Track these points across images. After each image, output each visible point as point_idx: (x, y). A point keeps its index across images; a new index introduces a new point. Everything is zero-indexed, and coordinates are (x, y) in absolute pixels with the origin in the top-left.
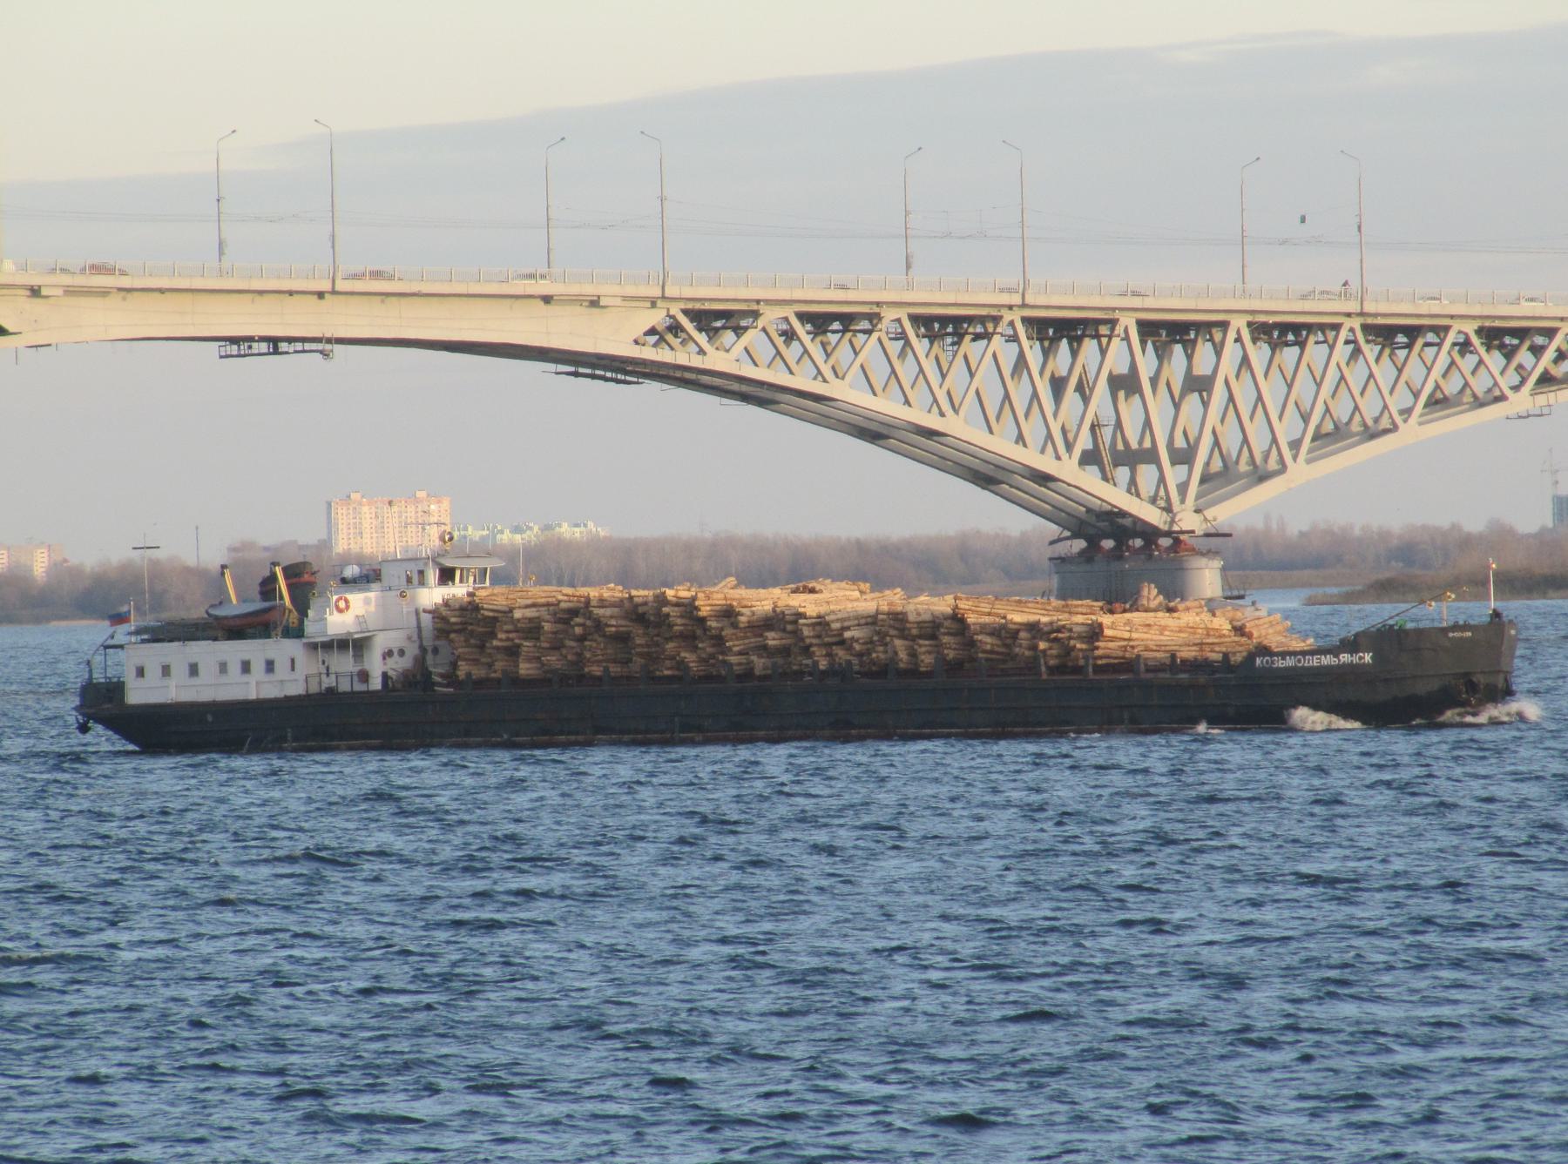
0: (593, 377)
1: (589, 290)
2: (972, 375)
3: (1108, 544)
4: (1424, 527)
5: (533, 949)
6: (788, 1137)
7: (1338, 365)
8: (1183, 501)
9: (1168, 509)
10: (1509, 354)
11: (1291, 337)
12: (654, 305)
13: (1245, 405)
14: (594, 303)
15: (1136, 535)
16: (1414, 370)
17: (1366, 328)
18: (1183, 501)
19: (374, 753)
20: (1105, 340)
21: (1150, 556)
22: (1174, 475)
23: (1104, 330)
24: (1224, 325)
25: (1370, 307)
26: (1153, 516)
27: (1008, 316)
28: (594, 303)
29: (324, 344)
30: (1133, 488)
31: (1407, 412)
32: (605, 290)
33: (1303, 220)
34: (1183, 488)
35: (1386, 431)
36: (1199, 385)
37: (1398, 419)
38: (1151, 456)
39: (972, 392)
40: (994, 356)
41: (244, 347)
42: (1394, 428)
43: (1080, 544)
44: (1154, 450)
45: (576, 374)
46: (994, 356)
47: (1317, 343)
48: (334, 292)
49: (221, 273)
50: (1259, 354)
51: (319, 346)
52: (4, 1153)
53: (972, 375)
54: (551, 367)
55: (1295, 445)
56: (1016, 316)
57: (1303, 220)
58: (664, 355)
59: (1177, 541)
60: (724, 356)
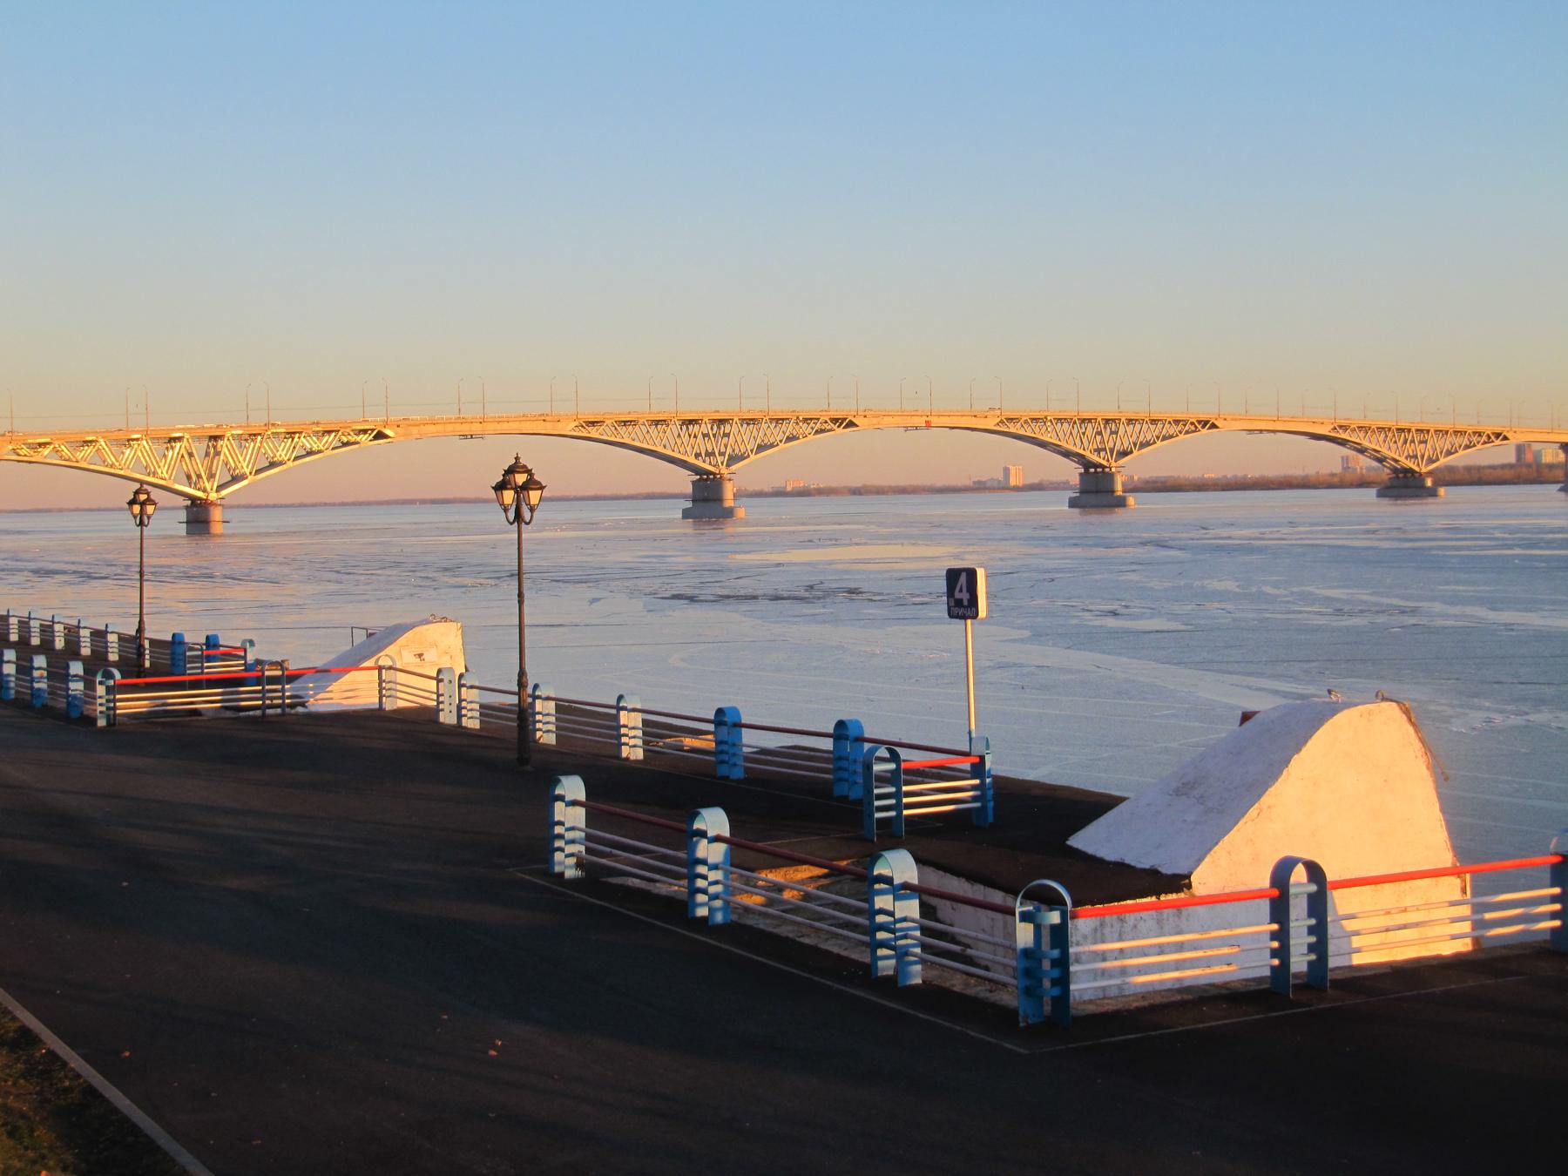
1: (1321, 421)
4: (1285, 477)
6: (14, 563)
9: (1108, 460)
10: (808, 424)
13: (739, 441)
14: (1322, 423)
15: (1409, 472)
16: (784, 428)
19: (1387, 499)
21: (1415, 477)
22: (720, 459)
23: (1117, 421)
24: (702, 420)
26: (1417, 469)
28: (1322, 423)
32: (1325, 421)
34: (722, 463)
36: (728, 435)
42: (778, 445)
43: (1394, 475)
44: (714, 453)
52: (9, 543)
56: (1076, 418)
60: (594, 432)
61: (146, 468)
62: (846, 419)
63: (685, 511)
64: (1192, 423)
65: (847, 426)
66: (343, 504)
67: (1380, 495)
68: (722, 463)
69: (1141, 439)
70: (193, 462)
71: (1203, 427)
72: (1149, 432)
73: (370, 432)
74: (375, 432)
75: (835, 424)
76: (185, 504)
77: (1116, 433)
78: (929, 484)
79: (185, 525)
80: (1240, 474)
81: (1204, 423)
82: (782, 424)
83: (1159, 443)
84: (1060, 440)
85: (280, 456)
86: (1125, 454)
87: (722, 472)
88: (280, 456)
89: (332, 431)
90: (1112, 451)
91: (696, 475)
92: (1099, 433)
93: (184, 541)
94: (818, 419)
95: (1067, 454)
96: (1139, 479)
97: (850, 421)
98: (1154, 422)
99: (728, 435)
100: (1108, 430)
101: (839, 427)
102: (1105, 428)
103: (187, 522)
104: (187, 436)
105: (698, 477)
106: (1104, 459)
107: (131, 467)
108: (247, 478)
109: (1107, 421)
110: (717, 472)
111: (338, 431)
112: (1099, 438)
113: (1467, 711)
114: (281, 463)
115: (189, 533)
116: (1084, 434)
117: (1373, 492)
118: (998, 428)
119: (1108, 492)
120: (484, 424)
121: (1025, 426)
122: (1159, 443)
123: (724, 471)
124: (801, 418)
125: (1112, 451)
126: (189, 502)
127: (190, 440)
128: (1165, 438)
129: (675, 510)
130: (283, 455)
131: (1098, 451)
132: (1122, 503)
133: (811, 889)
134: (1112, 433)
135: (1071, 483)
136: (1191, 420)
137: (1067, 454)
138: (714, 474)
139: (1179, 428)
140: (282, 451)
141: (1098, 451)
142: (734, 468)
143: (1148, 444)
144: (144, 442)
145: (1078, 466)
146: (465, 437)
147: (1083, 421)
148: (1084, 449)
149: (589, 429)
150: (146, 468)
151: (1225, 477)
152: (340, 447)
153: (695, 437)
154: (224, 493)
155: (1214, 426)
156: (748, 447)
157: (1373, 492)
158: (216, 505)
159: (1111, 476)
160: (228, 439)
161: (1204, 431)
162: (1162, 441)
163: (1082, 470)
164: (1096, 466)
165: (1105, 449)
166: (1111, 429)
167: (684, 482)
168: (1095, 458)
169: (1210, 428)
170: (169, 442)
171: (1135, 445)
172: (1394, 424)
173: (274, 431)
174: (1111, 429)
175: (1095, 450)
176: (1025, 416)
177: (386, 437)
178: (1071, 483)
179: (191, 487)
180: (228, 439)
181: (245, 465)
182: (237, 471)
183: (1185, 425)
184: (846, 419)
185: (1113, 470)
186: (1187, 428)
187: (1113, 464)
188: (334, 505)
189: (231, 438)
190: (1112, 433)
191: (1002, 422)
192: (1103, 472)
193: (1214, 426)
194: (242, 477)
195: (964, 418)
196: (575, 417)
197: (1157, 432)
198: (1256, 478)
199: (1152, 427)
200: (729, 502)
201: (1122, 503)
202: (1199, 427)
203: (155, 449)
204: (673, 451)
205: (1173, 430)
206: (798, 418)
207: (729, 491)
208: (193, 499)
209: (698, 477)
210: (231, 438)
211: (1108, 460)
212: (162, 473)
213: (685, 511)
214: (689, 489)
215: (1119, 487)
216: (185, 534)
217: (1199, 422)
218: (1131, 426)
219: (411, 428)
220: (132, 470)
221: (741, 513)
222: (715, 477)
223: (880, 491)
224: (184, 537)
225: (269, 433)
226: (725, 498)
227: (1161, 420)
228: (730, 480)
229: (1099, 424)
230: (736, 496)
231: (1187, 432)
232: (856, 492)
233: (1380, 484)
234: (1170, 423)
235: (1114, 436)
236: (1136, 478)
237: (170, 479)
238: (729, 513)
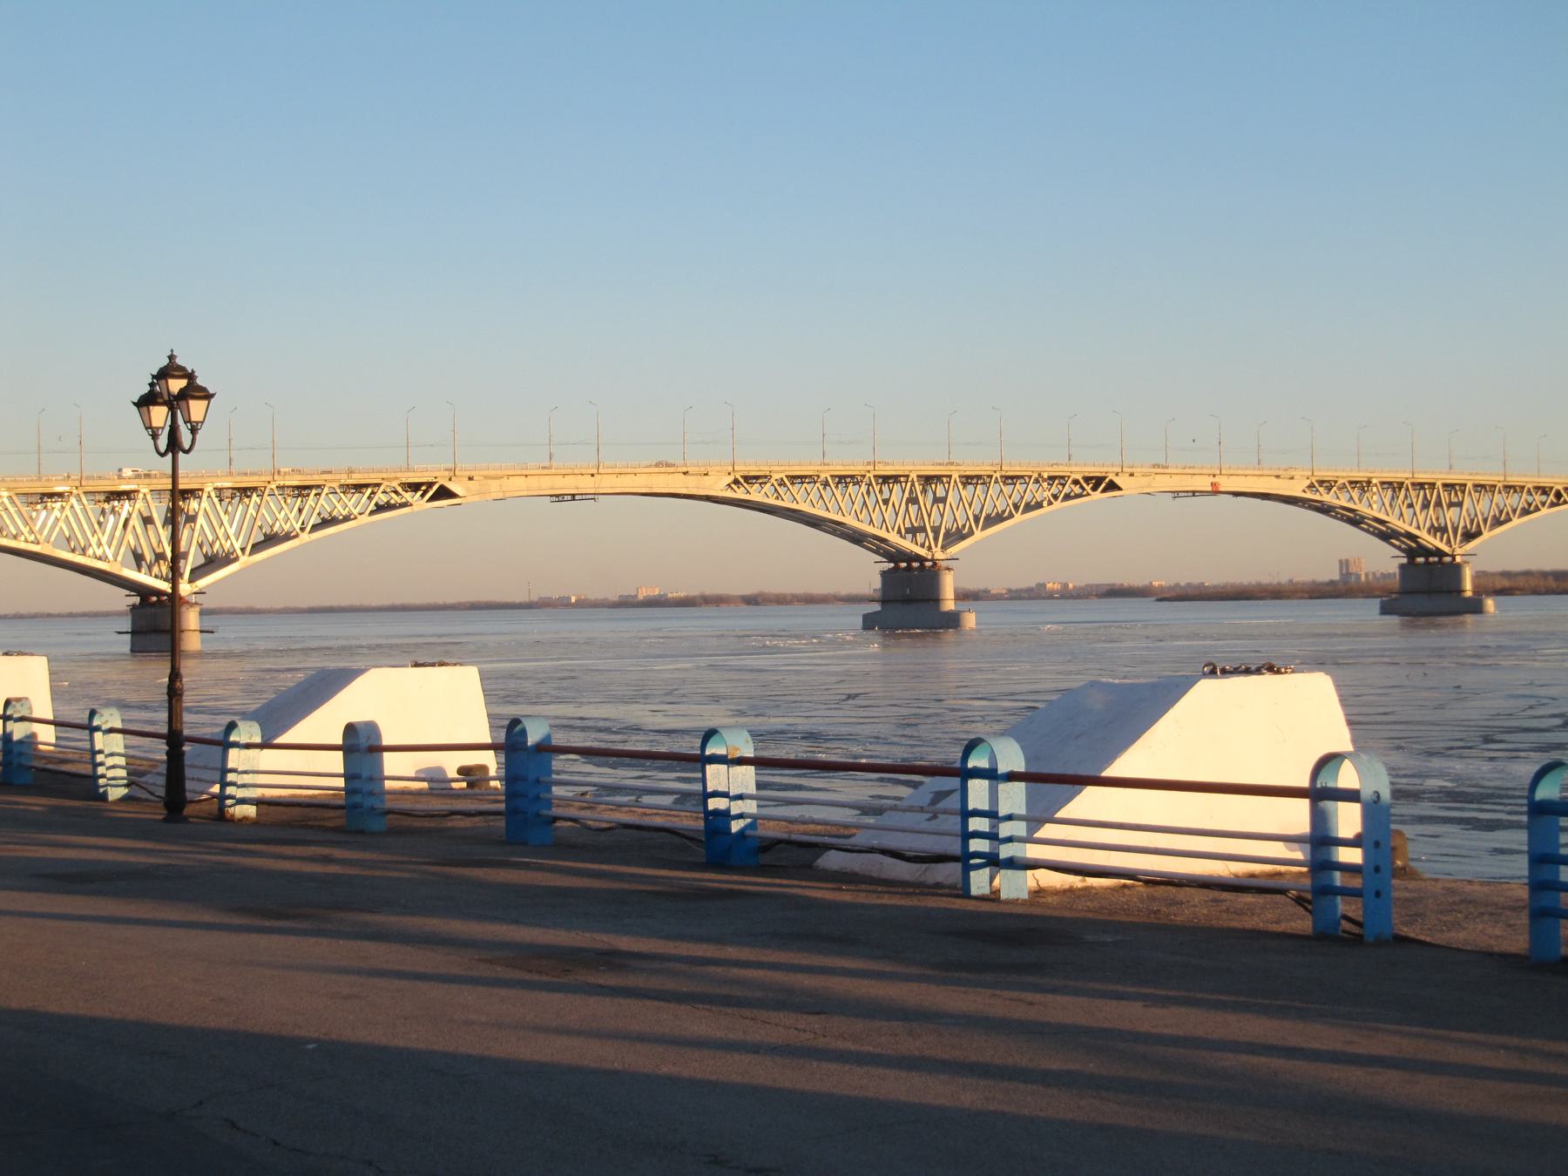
2: (853, 503)
3: (904, 565)
5: (339, 817)
7: (862, 494)
8: (936, 546)
9: (930, 548)
12: (729, 474)
17: (1413, 484)
18: (936, 546)
20: (903, 484)
23: (945, 480)
25: (1508, 479)
26: (923, 552)
27: (868, 475)
29: (593, 496)
33: (1194, 441)
35: (353, 519)
39: (853, 511)
40: (850, 494)
41: (560, 498)
46: (850, 494)
47: (1021, 484)
48: (1221, 474)
49: (1259, 469)
50: (1475, 495)
51: (593, 496)
53: (853, 503)
57: (1194, 441)
59: (935, 564)
60: (756, 494)
61: (68, 540)
62: (1105, 478)
63: (866, 618)
64: (1076, 482)
66: (71, 615)
67: (1386, 610)
69: (987, 509)
70: (151, 533)
71: (1094, 489)
72: (996, 498)
73: (424, 488)
74: (435, 488)
76: (131, 603)
77: (943, 500)
78: (358, 604)
79: (128, 637)
80: (1196, 581)
81: (1097, 482)
83: (1019, 517)
84: (1388, 515)
85: (287, 519)
86: (1469, 536)
87: (936, 557)
88: (287, 519)
89: (367, 486)
90: (936, 530)
91: (889, 562)
92: (913, 500)
93: (129, 665)
95: (857, 538)
96: (1074, 587)
97: (442, 488)
98: (1010, 479)
100: (930, 495)
101: (422, 496)
102: (924, 491)
103: (134, 633)
104: (144, 490)
105: (892, 565)
106: (923, 546)
107: (53, 539)
108: (236, 559)
109: (928, 480)
110: (930, 557)
111: (378, 485)
112: (913, 509)
114: (288, 537)
115: (135, 650)
116: (886, 502)
117: (1375, 604)
118: (729, 494)
119: (1450, 592)
120: (597, 477)
121: (781, 490)
122: (1018, 517)
123: (939, 555)
124: (1045, 475)
125: (1455, 530)
126: (137, 600)
127: (149, 497)
128: (1029, 508)
129: (853, 618)
130: (291, 516)
131: (913, 531)
132: (1475, 607)
134: (937, 500)
135: (992, 592)
136: (1074, 476)
137: (857, 538)
138: (921, 559)
139: (1054, 490)
140: (284, 515)
141: (913, 531)
142: (954, 550)
143: (1000, 518)
144: (73, 500)
145: (880, 558)
146: (559, 498)
147: (886, 479)
148: (1418, 528)
149: (794, 489)
150: (68, 540)
151: (1177, 585)
152: (867, 506)
154: (202, 583)
155: (1112, 486)
157: (1375, 604)
158: (192, 605)
159: (1455, 570)
160: (209, 497)
161: (1097, 495)
162: (1023, 513)
163: (1405, 561)
164: (1427, 552)
165: (923, 529)
166: (935, 493)
167: (866, 573)
168: (907, 545)
169: (1104, 491)
170: (108, 500)
171: (977, 519)
172: (1502, 479)
173: (282, 483)
174: (935, 493)
175: (907, 530)
176: (1343, 477)
177: (452, 495)
178: (992, 592)
179: (139, 571)
180: (209, 497)
181: (231, 532)
182: (217, 546)
183: (1064, 485)
184: (1105, 478)
185: (1458, 559)
186: (1066, 490)
187: (1458, 551)
188: (60, 616)
189: (213, 494)
190: (937, 500)
191: (736, 482)
192: (909, 568)
193: (1112, 486)
194: (228, 559)
195: (1262, 478)
196: (731, 469)
197: (1016, 497)
198: (1245, 586)
199: (1007, 489)
200: (949, 605)
201: (953, 620)
202: (1088, 488)
203: (91, 509)
205: (1044, 493)
206: (1039, 475)
207: (949, 587)
208: (143, 591)
209: (892, 565)
210: (213, 494)
211: (1449, 542)
212: (100, 544)
213: (866, 618)
214: (877, 583)
215: (1468, 586)
216: (129, 652)
217: (1087, 479)
218: (970, 488)
219: (490, 481)
220: (56, 545)
221: (970, 620)
222: (922, 565)
223: (781, 600)
224: (115, 658)
225: (274, 486)
226: (184, 626)
227: (1022, 477)
228: (948, 569)
229: (913, 485)
230: (962, 596)
231: (1067, 497)
232: (751, 601)
235: (941, 506)
236: (1071, 586)
237: (116, 555)
238: (953, 621)
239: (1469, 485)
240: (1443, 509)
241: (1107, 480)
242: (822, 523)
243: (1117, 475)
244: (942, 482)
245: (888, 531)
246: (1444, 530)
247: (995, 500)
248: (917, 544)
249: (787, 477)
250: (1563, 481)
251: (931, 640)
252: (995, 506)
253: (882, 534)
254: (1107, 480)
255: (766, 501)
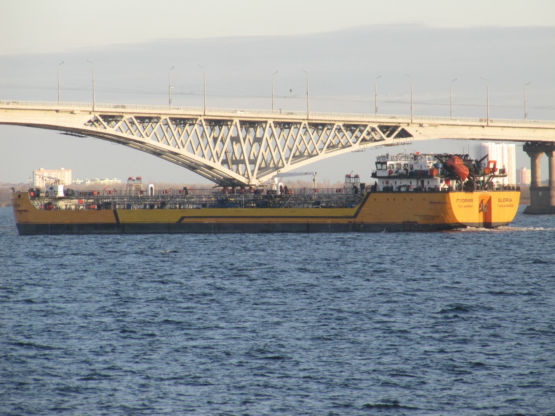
0: (72, 135)
9: (248, 178)
11: (287, 126)
14: (72, 113)
15: (238, 186)
17: (310, 124)
18: (253, 176)
20: (229, 126)
23: (229, 123)
25: (310, 117)
26: (243, 180)
30: (237, 171)
31: (321, 149)
33: (291, 91)
34: (253, 172)
36: (258, 140)
37: (319, 152)
38: (243, 162)
42: (318, 154)
44: (244, 160)
45: (66, 134)
47: (294, 128)
48: (488, 126)
54: (59, 132)
55: (287, 159)
57: (291, 91)
58: (93, 129)
60: (111, 130)
65: (399, 136)
68: (253, 172)
75: (384, 132)
82: (323, 130)
94: (366, 126)
99: (258, 140)
101: (388, 136)
106: (243, 175)
113: (66, 340)
133: (209, 410)
136: (370, 125)
138: (242, 185)
153: (222, 141)
156: (283, 154)
172: (305, 117)
183: (361, 132)
184: (397, 127)
204: (203, 156)
209: (222, 188)
233: (34, 182)
234: (339, 130)
239: (270, 122)
240: (260, 146)
241: (400, 129)
242: (164, 153)
243: (408, 125)
244: (227, 125)
245: (214, 162)
246: (236, 162)
247: (315, 144)
248: (239, 174)
249: (171, 119)
250: (343, 119)
251: (213, 236)
252: (306, 148)
253: (210, 163)
254: (400, 129)
255: (119, 134)
